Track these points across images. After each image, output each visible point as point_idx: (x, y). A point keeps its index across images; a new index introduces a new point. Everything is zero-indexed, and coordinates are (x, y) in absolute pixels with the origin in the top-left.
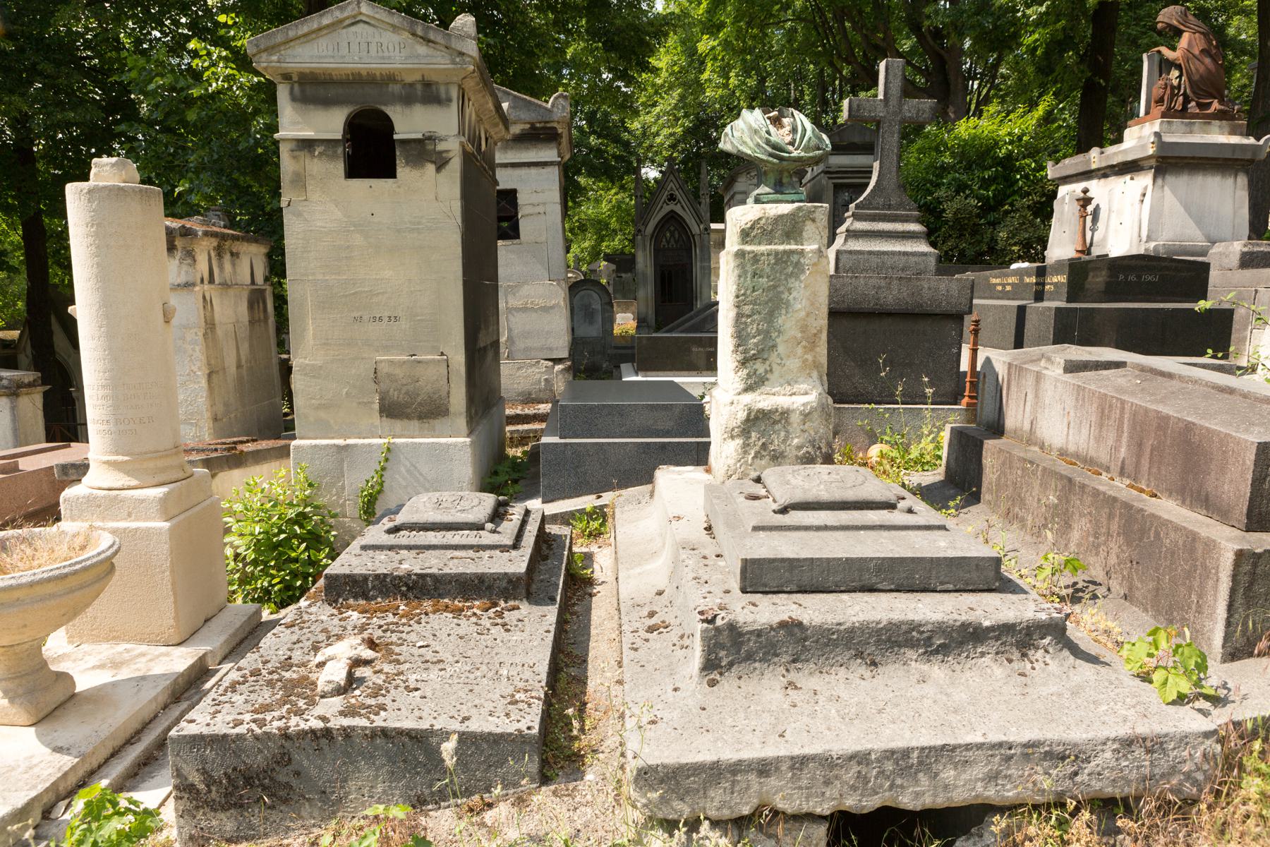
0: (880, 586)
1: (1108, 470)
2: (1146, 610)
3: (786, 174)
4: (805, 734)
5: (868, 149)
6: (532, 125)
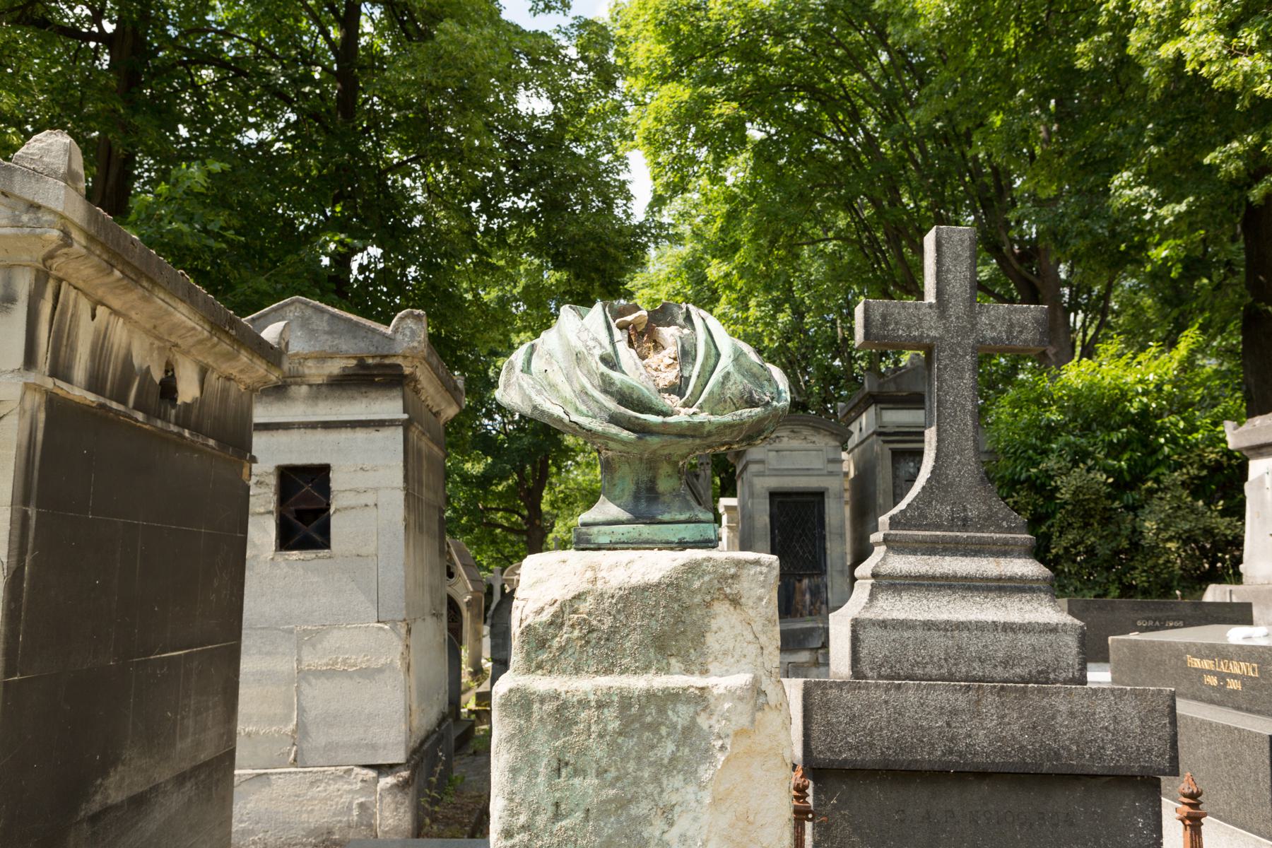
3: (665, 469)
5: (915, 401)
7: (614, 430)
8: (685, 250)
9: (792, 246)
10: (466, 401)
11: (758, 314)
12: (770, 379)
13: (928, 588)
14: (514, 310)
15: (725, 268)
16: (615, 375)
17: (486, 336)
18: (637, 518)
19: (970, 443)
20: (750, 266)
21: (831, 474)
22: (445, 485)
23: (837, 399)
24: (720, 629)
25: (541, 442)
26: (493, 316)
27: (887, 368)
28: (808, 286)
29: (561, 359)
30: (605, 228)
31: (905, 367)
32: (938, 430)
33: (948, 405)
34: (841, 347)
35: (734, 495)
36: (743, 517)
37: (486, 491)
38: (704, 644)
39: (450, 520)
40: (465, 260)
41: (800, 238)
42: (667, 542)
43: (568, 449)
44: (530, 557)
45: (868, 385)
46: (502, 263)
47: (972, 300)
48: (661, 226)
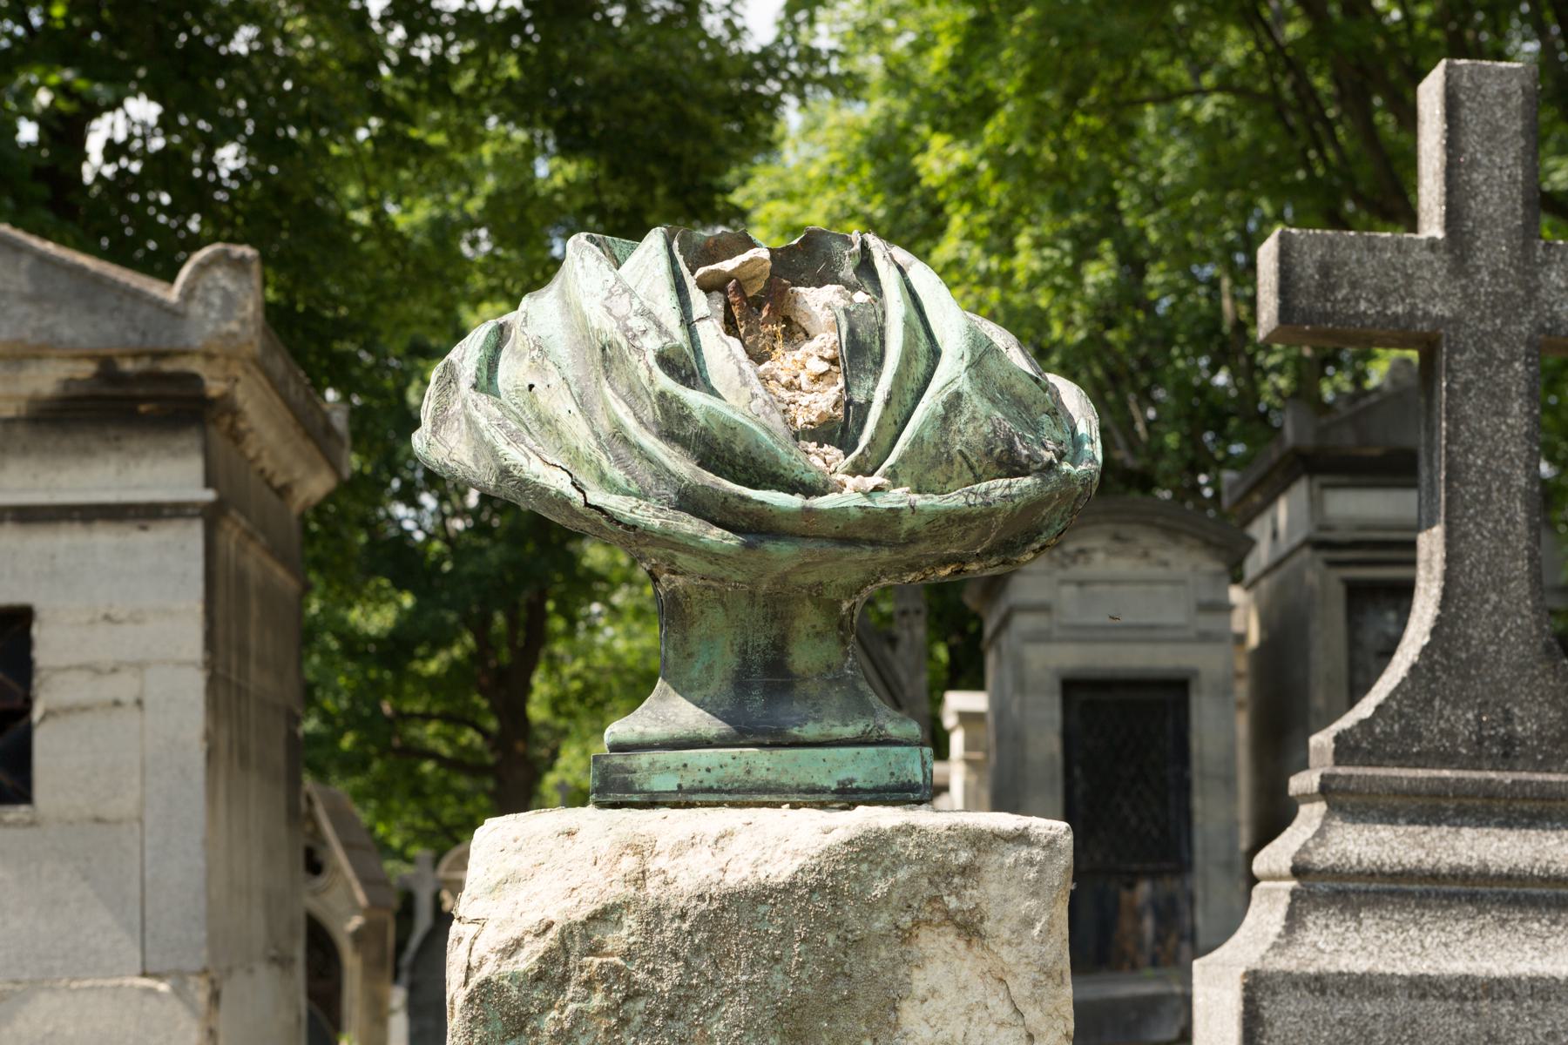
3: (808, 618)
5: (1398, 468)
6: (107, 365)
7: (689, 525)
8: (866, 113)
9: (1117, 106)
10: (353, 462)
11: (1036, 265)
12: (1057, 411)
13: (1423, 900)
14: (466, 249)
15: (961, 156)
16: (694, 399)
17: (402, 310)
18: (742, 732)
19: (1523, 565)
20: (1020, 153)
21: (1205, 637)
22: (301, 660)
23: (1221, 465)
24: (933, 992)
25: (527, 558)
26: (419, 265)
27: (1337, 390)
28: (1153, 198)
29: (566, 361)
30: (680, 60)
31: (1377, 390)
32: (1449, 534)
33: (1472, 475)
34: (1230, 343)
35: (977, 684)
36: (1000, 738)
37: (401, 673)
38: (896, 1026)
39: (313, 740)
40: (351, 131)
41: (1138, 87)
42: (813, 790)
43: (593, 576)
44: (491, 823)
45: (1292, 429)
46: (438, 139)
47: (1529, 232)
48: (811, 56)
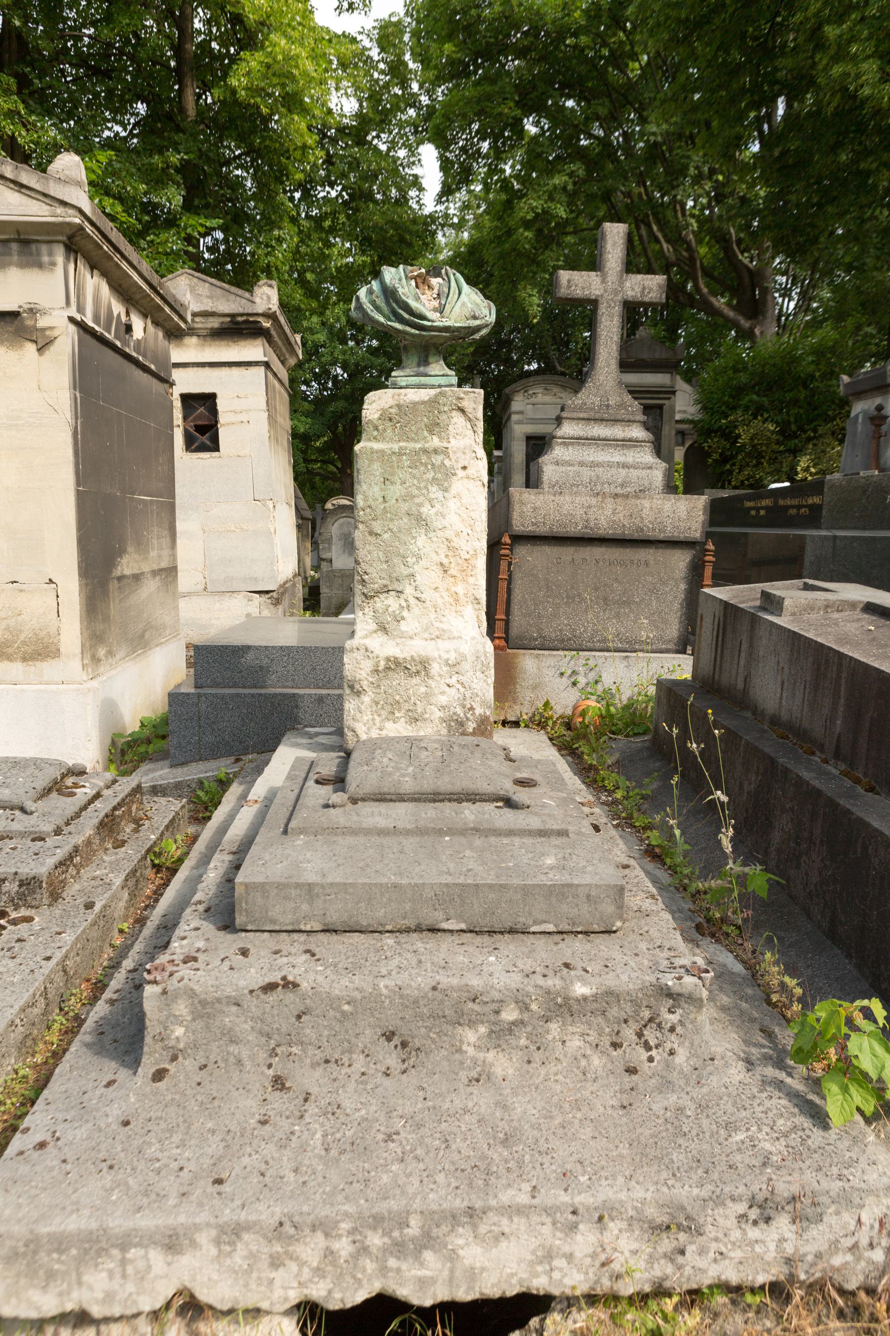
0: (445, 926)
1: (822, 750)
2: (849, 956)
4: (255, 1179)
